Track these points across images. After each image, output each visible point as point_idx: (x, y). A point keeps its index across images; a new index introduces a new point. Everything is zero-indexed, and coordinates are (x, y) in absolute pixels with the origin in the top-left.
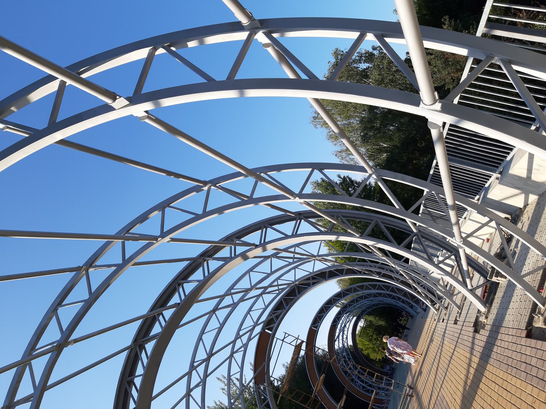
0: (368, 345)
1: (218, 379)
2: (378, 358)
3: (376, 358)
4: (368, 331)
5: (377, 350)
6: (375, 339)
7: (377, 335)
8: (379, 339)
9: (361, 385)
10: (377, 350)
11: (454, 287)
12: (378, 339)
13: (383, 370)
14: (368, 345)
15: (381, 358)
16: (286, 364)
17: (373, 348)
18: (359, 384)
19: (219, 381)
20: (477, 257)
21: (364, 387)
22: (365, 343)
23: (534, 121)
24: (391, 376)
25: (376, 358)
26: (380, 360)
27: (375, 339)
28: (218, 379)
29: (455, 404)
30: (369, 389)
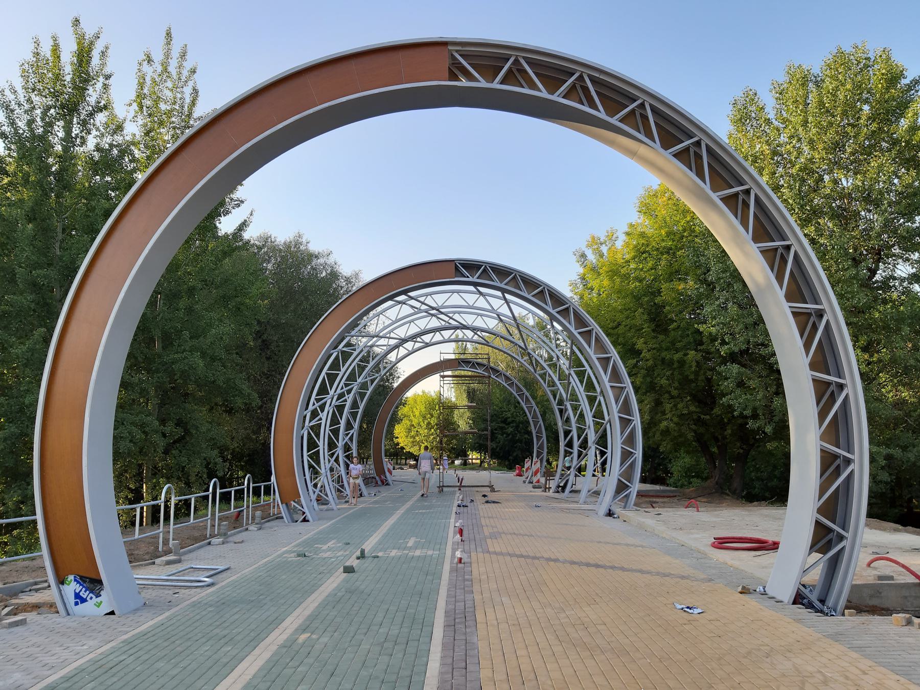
0: (414, 416)
1: (169, 35)
2: (400, 440)
3: (397, 438)
4: (437, 406)
5: (412, 434)
6: (429, 423)
7: (437, 425)
8: (433, 430)
9: (346, 401)
10: (412, 434)
11: (782, 530)
12: (431, 429)
13: (383, 457)
14: (414, 416)
15: (401, 445)
16: (304, 240)
17: (413, 425)
18: (347, 396)
19: (163, 41)
20: (771, 538)
21: (340, 408)
22: (415, 409)
23: (784, 503)
24: (379, 482)
25: (397, 438)
26: (398, 444)
27: (429, 423)
28: (169, 35)
29: (355, 609)
30: (359, 408)
